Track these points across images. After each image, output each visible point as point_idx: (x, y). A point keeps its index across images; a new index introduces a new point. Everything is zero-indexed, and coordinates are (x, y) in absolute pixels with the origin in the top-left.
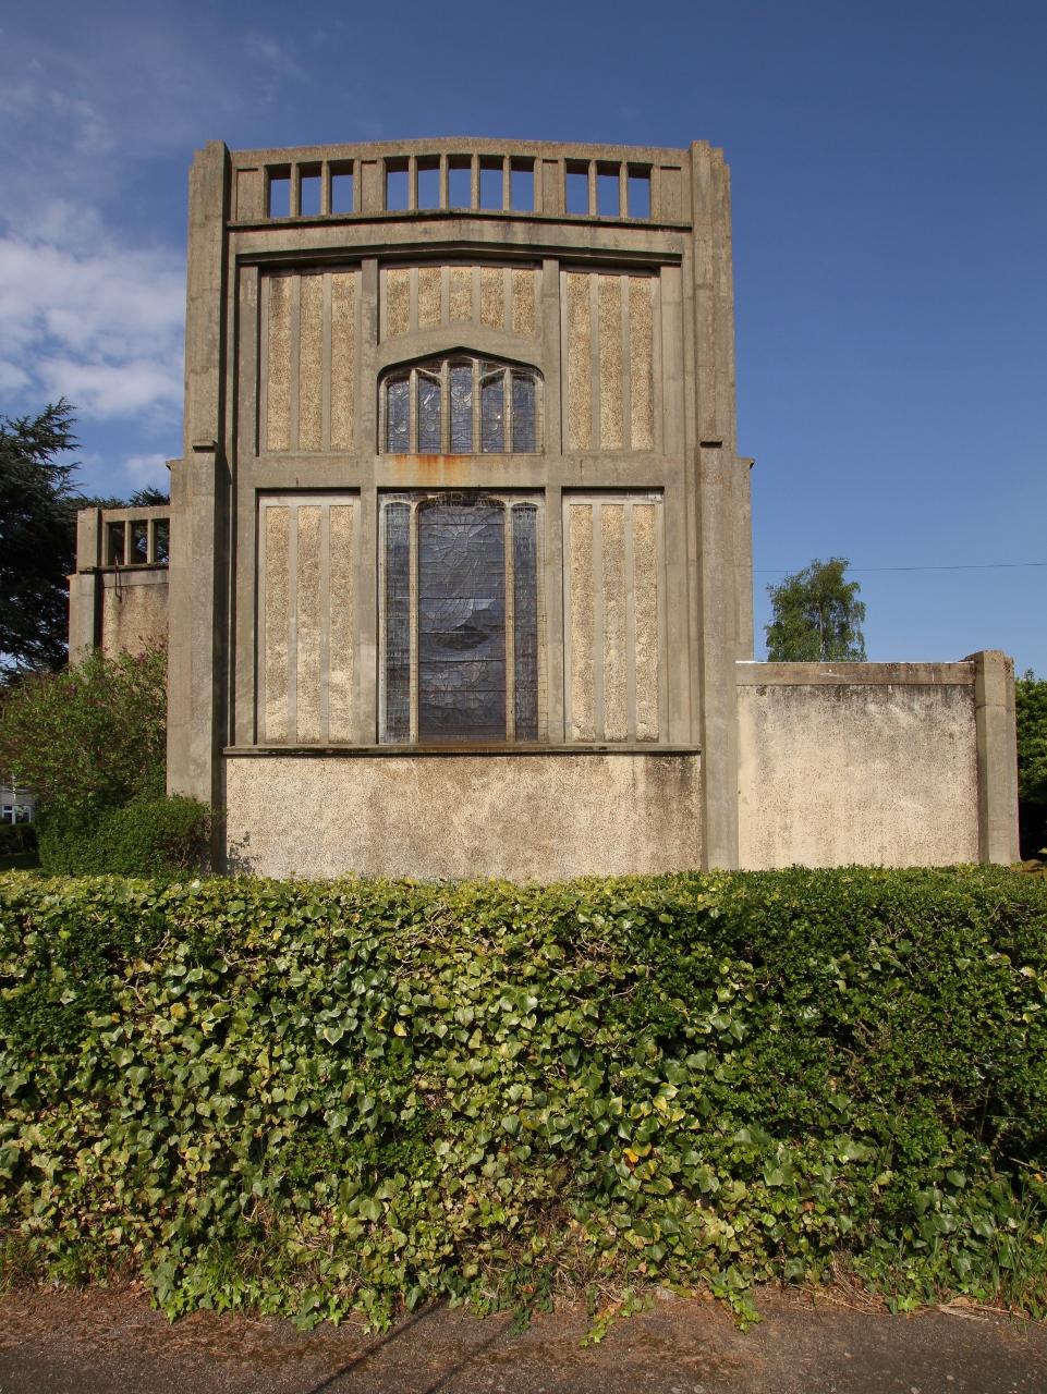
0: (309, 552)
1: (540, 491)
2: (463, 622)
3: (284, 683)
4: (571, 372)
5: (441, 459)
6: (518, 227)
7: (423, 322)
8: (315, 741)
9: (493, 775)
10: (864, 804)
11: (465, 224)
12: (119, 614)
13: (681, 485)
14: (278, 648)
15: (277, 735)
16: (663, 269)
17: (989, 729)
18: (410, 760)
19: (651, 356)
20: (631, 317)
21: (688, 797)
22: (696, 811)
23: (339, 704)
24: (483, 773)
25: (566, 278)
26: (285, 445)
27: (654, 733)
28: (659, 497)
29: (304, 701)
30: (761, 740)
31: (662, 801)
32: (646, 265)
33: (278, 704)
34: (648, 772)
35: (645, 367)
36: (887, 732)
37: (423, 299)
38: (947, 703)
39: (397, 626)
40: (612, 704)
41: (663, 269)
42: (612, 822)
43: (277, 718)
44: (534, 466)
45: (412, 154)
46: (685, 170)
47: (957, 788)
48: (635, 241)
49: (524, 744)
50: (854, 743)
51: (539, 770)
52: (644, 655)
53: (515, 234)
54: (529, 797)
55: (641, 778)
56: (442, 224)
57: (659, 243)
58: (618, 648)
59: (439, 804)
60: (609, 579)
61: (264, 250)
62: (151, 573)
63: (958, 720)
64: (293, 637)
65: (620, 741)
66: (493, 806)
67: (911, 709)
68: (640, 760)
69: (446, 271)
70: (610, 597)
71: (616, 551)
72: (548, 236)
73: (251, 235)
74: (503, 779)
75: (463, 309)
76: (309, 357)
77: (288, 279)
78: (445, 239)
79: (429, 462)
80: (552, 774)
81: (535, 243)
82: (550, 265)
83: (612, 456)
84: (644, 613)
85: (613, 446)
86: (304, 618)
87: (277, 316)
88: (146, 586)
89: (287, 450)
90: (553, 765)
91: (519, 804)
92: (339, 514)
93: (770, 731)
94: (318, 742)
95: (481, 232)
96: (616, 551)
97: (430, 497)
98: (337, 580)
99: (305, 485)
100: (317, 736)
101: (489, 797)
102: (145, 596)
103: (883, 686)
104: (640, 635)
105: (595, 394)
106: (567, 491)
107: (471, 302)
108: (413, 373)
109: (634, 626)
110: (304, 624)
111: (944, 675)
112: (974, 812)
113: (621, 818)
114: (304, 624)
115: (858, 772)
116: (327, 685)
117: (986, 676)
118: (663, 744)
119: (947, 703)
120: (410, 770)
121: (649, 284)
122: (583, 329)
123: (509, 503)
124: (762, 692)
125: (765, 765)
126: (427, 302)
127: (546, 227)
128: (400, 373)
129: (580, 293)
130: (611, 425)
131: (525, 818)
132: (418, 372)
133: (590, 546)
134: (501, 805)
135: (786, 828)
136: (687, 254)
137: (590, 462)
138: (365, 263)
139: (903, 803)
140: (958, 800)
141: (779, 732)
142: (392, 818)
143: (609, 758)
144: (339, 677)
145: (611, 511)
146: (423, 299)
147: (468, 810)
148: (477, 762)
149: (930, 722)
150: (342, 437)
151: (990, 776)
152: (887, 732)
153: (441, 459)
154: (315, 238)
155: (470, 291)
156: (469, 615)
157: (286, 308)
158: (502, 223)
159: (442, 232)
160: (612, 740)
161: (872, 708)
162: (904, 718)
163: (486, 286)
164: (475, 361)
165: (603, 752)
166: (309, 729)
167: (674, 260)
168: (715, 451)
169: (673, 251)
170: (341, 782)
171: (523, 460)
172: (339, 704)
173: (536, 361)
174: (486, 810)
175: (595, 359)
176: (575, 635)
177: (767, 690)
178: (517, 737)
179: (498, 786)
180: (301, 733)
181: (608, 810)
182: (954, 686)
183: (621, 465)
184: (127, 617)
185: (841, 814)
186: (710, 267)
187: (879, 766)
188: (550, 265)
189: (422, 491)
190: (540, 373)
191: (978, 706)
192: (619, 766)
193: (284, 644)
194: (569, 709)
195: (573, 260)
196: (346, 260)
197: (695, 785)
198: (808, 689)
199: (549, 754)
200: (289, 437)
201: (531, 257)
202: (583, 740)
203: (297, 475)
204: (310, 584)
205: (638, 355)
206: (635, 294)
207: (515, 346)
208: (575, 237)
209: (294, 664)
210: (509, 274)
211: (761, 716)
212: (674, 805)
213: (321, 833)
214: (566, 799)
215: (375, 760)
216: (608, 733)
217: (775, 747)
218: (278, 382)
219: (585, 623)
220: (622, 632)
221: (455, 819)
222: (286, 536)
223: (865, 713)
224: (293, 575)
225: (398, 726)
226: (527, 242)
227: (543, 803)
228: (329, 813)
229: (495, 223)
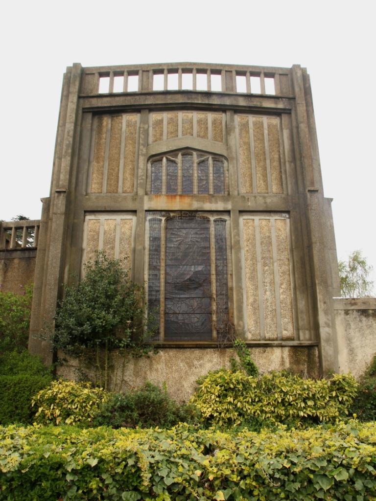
4: (242, 158)
16: (283, 115)
24: (201, 358)
40: (269, 321)
70: (265, 265)
74: (211, 361)
81: (222, 103)
92: (125, 223)
93: (353, 334)
104: (282, 284)
109: (278, 279)
132: (167, 158)
133: (254, 239)
145: (264, 223)
184: (9, 274)
211: (348, 326)
217: (357, 342)
219: (253, 278)
222: (98, 234)
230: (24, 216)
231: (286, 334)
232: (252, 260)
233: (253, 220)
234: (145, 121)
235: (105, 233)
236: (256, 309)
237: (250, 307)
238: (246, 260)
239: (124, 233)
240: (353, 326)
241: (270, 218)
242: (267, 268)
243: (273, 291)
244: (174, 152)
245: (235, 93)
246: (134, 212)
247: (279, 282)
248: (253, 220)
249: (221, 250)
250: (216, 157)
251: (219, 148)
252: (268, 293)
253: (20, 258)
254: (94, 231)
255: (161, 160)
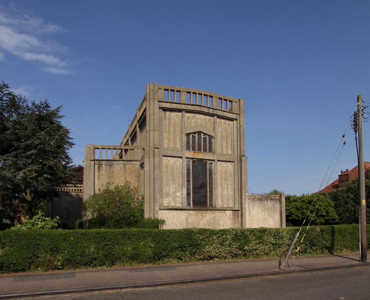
0: (172, 169)
1: (214, 160)
2: (200, 185)
3: (168, 195)
4: (219, 138)
5: (197, 153)
6: (211, 110)
7: (193, 125)
8: (173, 207)
9: (207, 214)
10: (264, 220)
11: (202, 108)
12: (99, 171)
13: (237, 161)
14: (166, 188)
15: (166, 205)
16: (234, 121)
17: (282, 207)
18: (193, 211)
19: (231, 136)
20: (228, 129)
21: (239, 218)
22: (240, 221)
23: (178, 200)
24: (206, 214)
25: (218, 120)
26: (167, 147)
27: (232, 206)
28: (233, 163)
29: (171, 199)
30: (249, 208)
31: (234, 219)
32: (231, 120)
33: (166, 199)
34: (232, 214)
35: (230, 138)
36: (268, 207)
37: (193, 120)
38: (276, 202)
39: (188, 185)
40: (225, 201)
41: (234, 121)
42: (227, 223)
43: (167, 202)
44: (213, 156)
45: (192, 92)
46: (238, 103)
47: (277, 217)
48: (230, 115)
49: (211, 208)
50: (263, 209)
51: (215, 213)
52: (231, 192)
53: (210, 111)
54: (213, 218)
55: (231, 215)
56: (198, 107)
57: (234, 116)
58: (226, 191)
59: (198, 219)
60: (225, 178)
61: (165, 107)
62: (107, 161)
63: (278, 205)
64: (169, 186)
65: (227, 208)
66: (207, 220)
67: (271, 203)
68: (231, 211)
69: (197, 115)
70: (225, 181)
71: (226, 173)
72: (216, 112)
73: (162, 103)
74: (209, 215)
75: (200, 123)
76: (172, 129)
77: (167, 112)
78: (198, 110)
79: (195, 153)
80: (217, 214)
81: (214, 113)
82: (215, 117)
83: (225, 154)
84: (231, 184)
85: (225, 153)
86: (171, 182)
87: (165, 120)
88: (106, 165)
89: (174, 148)
90: (217, 212)
91: (212, 219)
92: (178, 162)
93: (250, 206)
94: (174, 207)
95: (204, 110)
96: (226, 173)
97: (194, 160)
98: (178, 175)
99: (172, 156)
100: (174, 206)
101: (207, 218)
102: (106, 167)
103: (267, 199)
104: (230, 188)
105: (222, 142)
106: (219, 161)
107: (201, 122)
108: (191, 135)
109: (229, 187)
110: (171, 183)
111: (276, 197)
112: (280, 221)
113: (228, 222)
114: (171, 183)
115: (263, 214)
116: (176, 196)
117: (282, 198)
118: (234, 209)
119: (276, 202)
120: (193, 213)
121: (231, 123)
122: (220, 130)
123: (208, 162)
124: (249, 200)
125: (250, 212)
126: (193, 121)
127: (215, 110)
128: (189, 134)
129: (220, 123)
130: (225, 149)
131: (213, 222)
132: (192, 135)
133: (222, 171)
134: (208, 220)
135: (253, 224)
136: (238, 119)
137: (222, 156)
138: (183, 112)
139: (270, 219)
140: (278, 219)
141: (252, 207)
142: (190, 222)
143: (226, 211)
144: (178, 194)
145: (225, 165)
146: (193, 120)
147: (203, 220)
148: (205, 211)
149: (274, 205)
150: (178, 146)
151: (283, 215)
152: (268, 207)
153: (197, 153)
154: (174, 106)
155: (201, 120)
156: (201, 183)
157: (167, 118)
158: (208, 108)
159: (198, 109)
160: (225, 208)
161: (265, 203)
162: (270, 205)
163: (204, 119)
164: (202, 134)
165: (226, 210)
166: (172, 204)
167: (236, 120)
168: (244, 157)
169: (236, 118)
170: (181, 215)
171: (211, 154)
172: (178, 200)
173: (213, 136)
174: (206, 221)
175: (222, 136)
176: (219, 188)
177: (250, 199)
178: (210, 207)
179: (208, 216)
180: (171, 205)
181: (226, 221)
182: (277, 199)
183: (227, 157)
184: (101, 172)
185: (261, 221)
186: (243, 123)
187: (266, 213)
188: (215, 117)
189: (193, 158)
190: (214, 138)
191: (281, 203)
192: (228, 212)
193: (168, 187)
194: (219, 202)
195: (219, 117)
196: (180, 111)
197: (240, 216)
198: (256, 199)
199: (217, 210)
200: (168, 145)
201: (213, 115)
202: (221, 208)
203: (170, 153)
204: (173, 175)
205: (229, 136)
206: (224, 123)
207: (210, 132)
208: (220, 113)
209: (169, 191)
210: (208, 117)
211: (249, 204)
212: (236, 220)
213: (177, 225)
214: (219, 218)
215: (187, 211)
216: (225, 206)
217: (251, 210)
218: (166, 133)
219: (221, 186)
220: (227, 188)
221: (201, 222)
222: (168, 165)
223: (264, 204)
224: (169, 173)
225: (189, 204)
226: (212, 113)
227: (215, 219)
228: (178, 221)
229: (207, 108)
230: (278, 190)
231: (230, 206)
232: (221, 179)
233: (222, 164)
234: (183, 117)
235: (170, 165)
236: (222, 197)
237: (220, 196)
238: (219, 179)
239: (177, 166)
240: (250, 204)
241: (227, 163)
242: (225, 182)
243: (227, 191)
244: (195, 133)
245: (357, 168)
246: (181, 157)
247: (229, 188)
248: (222, 164)
249: (211, 174)
250: (210, 136)
251: (212, 134)
252: (225, 191)
253: (106, 165)
254: (166, 164)
255: (190, 136)
